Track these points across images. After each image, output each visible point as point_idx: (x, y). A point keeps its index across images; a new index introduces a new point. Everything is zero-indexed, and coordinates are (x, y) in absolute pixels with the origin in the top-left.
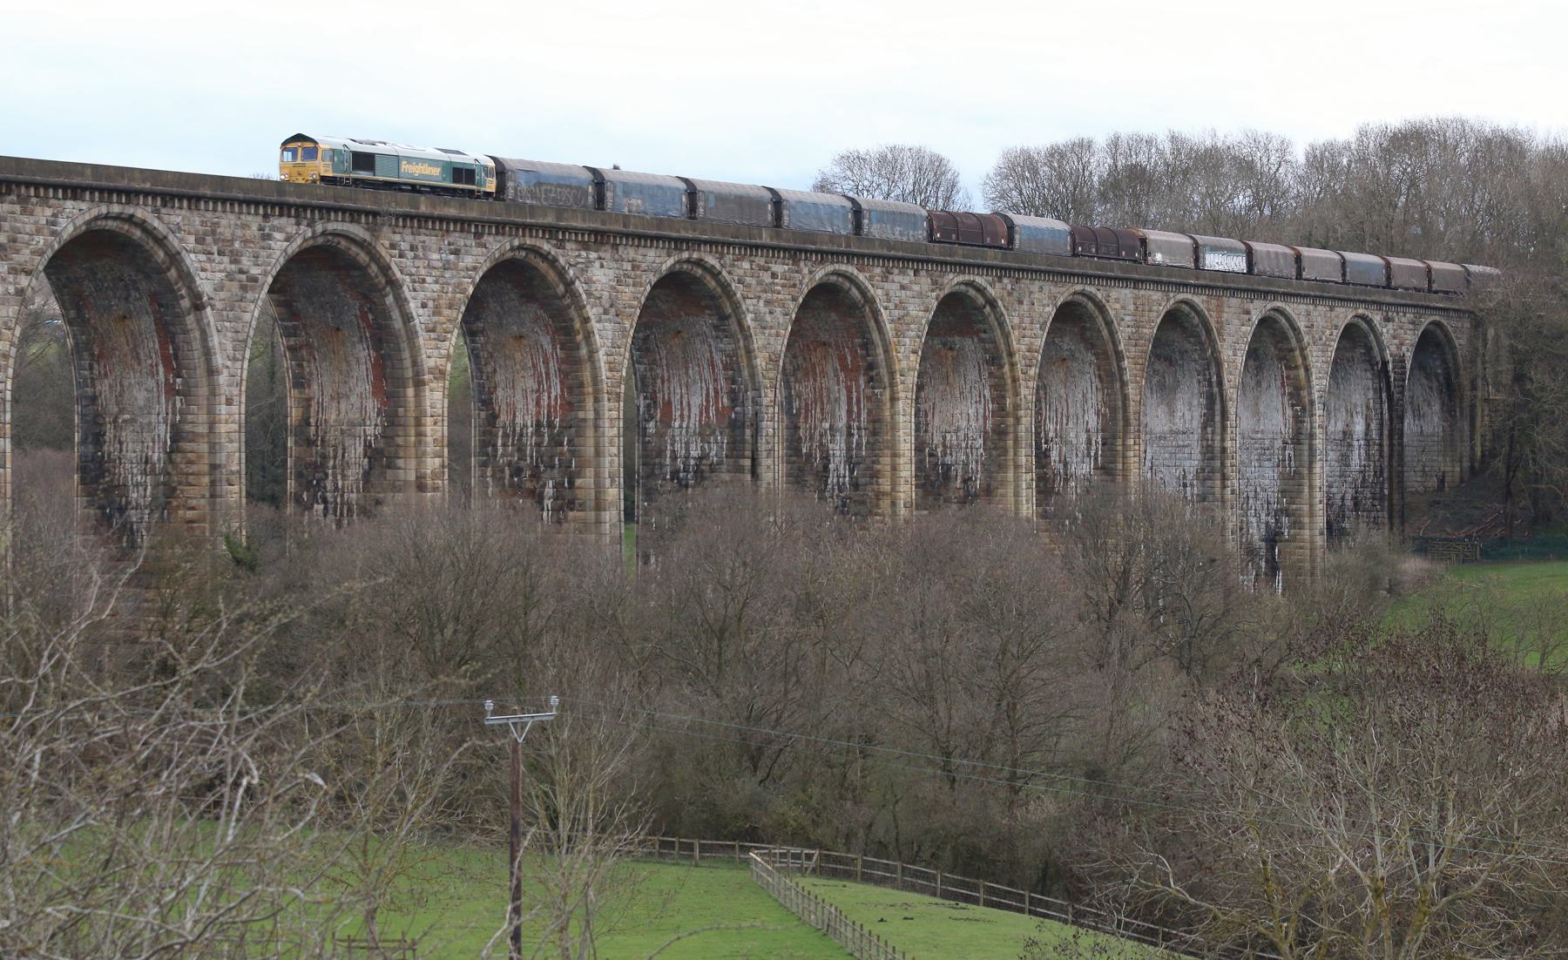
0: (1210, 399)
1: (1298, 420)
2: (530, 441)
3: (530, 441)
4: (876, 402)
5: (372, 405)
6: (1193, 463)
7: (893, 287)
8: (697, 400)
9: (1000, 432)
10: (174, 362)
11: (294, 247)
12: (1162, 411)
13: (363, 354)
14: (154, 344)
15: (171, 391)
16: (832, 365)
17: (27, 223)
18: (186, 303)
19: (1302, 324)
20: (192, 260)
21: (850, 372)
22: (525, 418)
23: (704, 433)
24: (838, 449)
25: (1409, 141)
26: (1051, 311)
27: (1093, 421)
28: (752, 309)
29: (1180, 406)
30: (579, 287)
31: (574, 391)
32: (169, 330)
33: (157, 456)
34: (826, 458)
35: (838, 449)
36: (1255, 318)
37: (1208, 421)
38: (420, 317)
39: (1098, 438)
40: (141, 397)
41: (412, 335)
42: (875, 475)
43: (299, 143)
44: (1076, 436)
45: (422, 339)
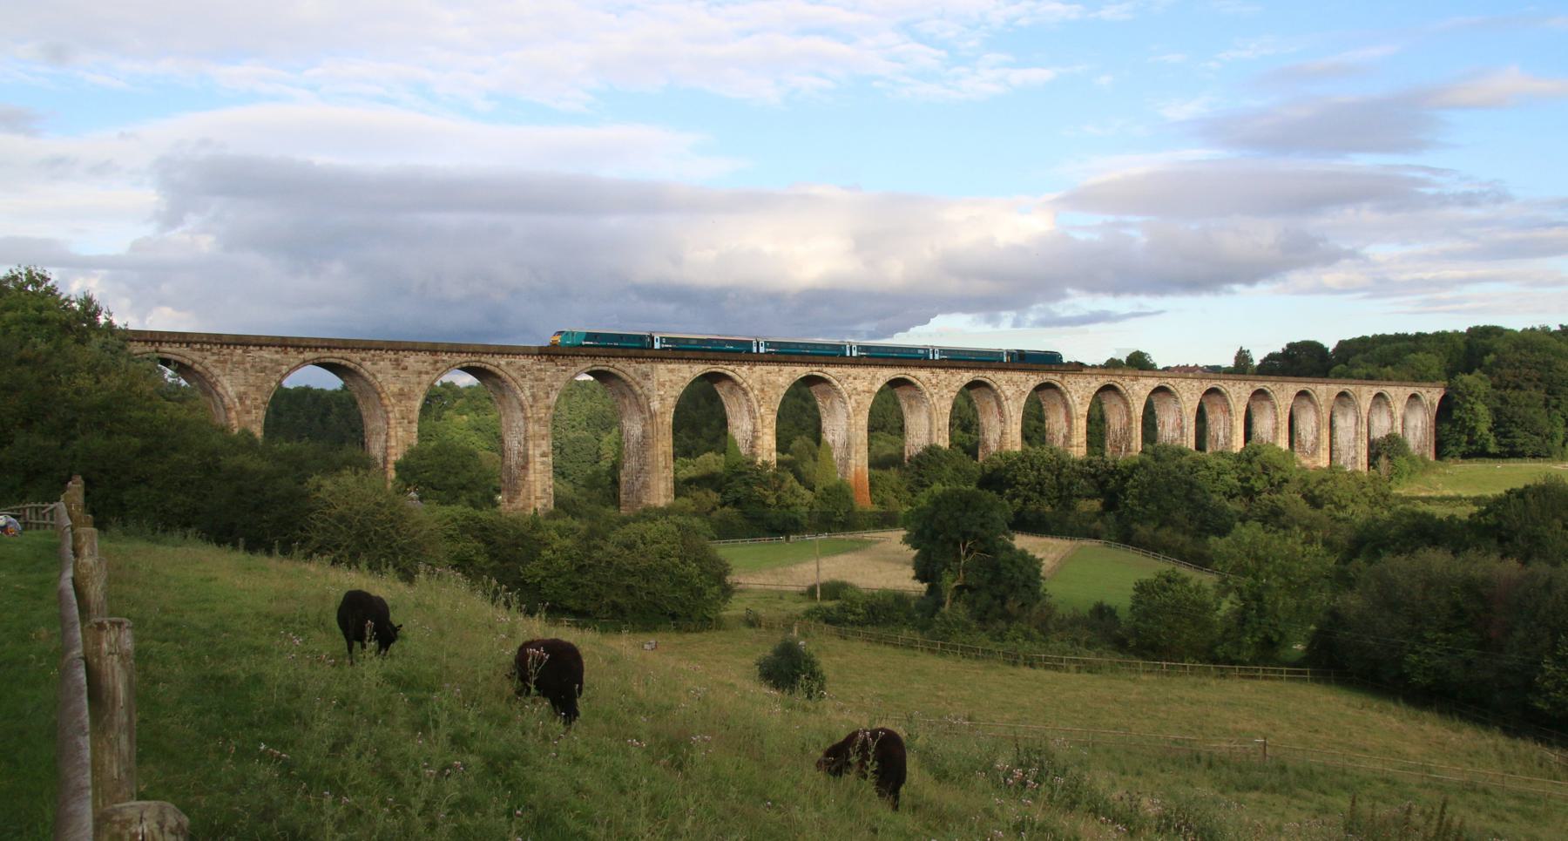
0: (1357, 418)
1: (1392, 423)
2: (1119, 433)
3: (1119, 433)
4: (1231, 421)
5: (1065, 424)
6: (1352, 436)
7: (1236, 388)
8: (1171, 421)
9: (1277, 428)
10: (1001, 413)
11: (1037, 383)
12: (1343, 421)
13: (1062, 411)
14: (995, 409)
15: (1001, 422)
16: (1219, 410)
17: (953, 379)
18: (1003, 398)
19: (1393, 395)
20: (1004, 387)
21: (1224, 412)
22: (1118, 427)
23: (1173, 430)
24: (1221, 434)
25: (322, 390)
26: (1295, 393)
27: (1313, 424)
28: (1185, 396)
29: (1348, 420)
30: (1130, 391)
31: (1130, 420)
32: (1000, 405)
33: (997, 438)
34: (1218, 436)
35: (1221, 434)
36: (1374, 393)
37: (1356, 424)
38: (1077, 401)
39: (1315, 429)
40: (993, 423)
41: (1075, 405)
42: (1231, 441)
43: (1561, 326)
44: (1309, 429)
45: (1078, 406)
